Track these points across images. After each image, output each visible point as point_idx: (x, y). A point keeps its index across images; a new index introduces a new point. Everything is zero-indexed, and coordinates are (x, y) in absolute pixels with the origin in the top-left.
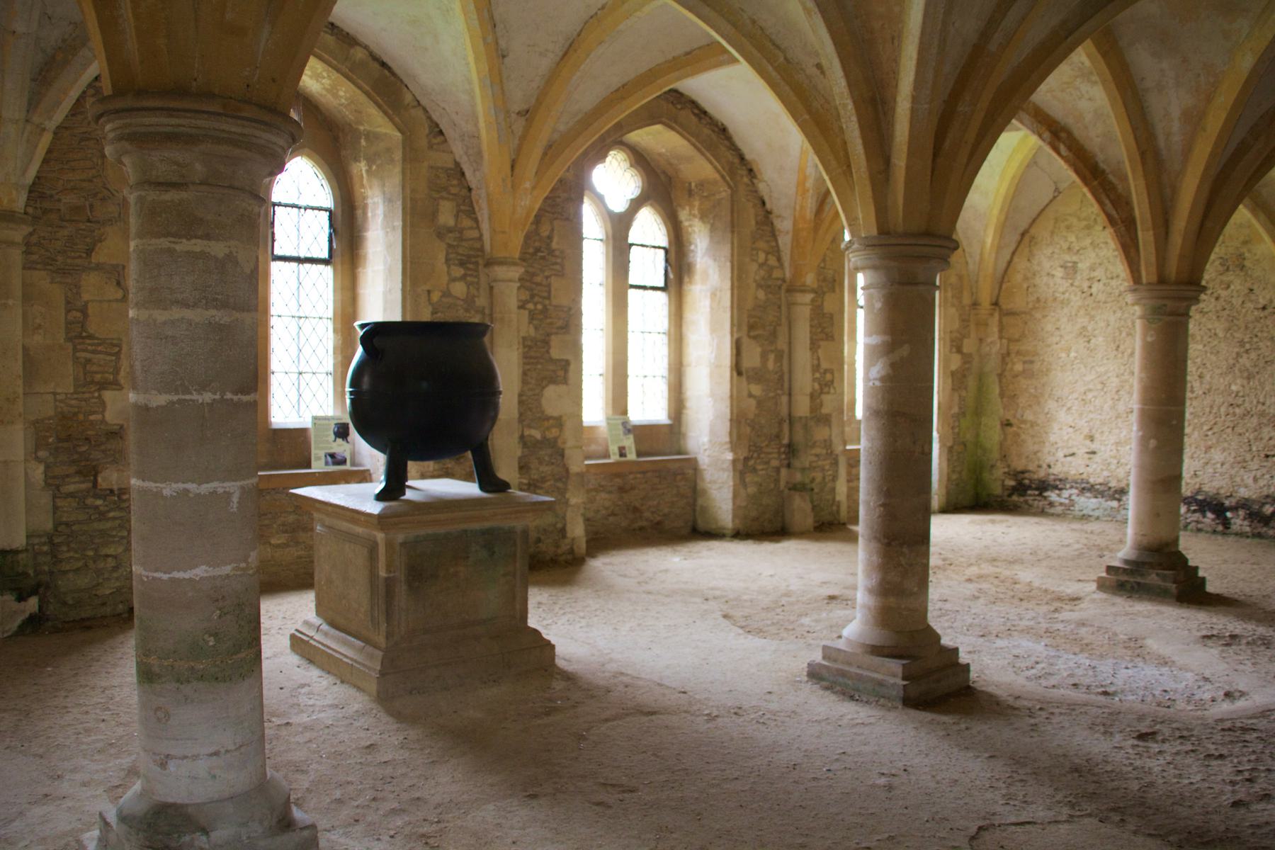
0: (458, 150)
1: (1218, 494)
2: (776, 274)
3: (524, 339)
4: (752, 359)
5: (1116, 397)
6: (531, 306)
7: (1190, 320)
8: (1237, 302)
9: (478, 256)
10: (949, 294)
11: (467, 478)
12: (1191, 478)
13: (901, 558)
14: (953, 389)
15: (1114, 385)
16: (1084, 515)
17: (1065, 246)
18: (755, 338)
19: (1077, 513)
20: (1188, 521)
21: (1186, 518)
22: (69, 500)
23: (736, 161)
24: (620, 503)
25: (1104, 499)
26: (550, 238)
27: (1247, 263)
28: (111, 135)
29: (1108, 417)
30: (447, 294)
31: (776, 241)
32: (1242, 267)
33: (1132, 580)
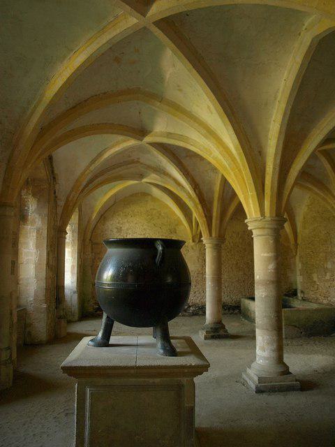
7: (183, 250)
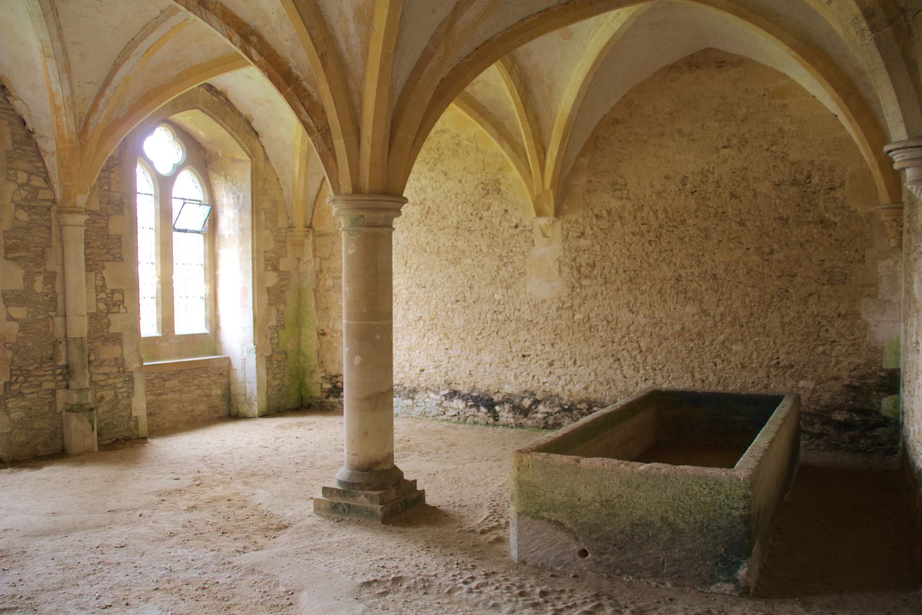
1: (488, 390)
2: (42, 195)
5: (406, 307)
8: (496, 221)
10: (263, 218)
12: (467, 377)
14: (269, 304)
15: (404, 296)
20: (467, 415)
21: (465, 413)
27: (502, 188)
29: (401, 325)
32: (499, 191)
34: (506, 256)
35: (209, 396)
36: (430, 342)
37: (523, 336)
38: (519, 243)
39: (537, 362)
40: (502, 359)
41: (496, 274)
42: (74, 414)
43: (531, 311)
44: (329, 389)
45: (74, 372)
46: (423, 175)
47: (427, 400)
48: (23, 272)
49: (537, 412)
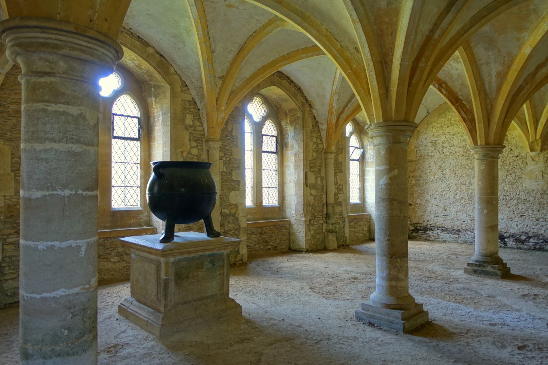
0: (194, 93)
2: (320, 146)
3: (222, 172)
4: (312, 180)
6: (224, 159)
9: (202, 138)
11: (200, 230)
13: (397, 264)
16: (444, 241)
17: (432, 134)
18: (312, 172)
19: (441, 240)
22: (11, 245)
23: (305, 101)
24: (260, 239)
25: (452, 234)
26: (232, 131)
28: (10, 44)
30: (189, 153)
31: (320, 133)
33: (480, 269)
34: (511, 170)
35: (363, 230)
36: (468, 209)
37: (520, 206)
38: (519, 164)
39: (529, 219)
40: (509, 217)
41: (505, 178)
42: (330, 233)
43: (525, 195)
44: (413, 229)
45: (330, 217)
46: (464, 134)
47: (466, 235)
48: (314, 176)
49: (529, 242)
